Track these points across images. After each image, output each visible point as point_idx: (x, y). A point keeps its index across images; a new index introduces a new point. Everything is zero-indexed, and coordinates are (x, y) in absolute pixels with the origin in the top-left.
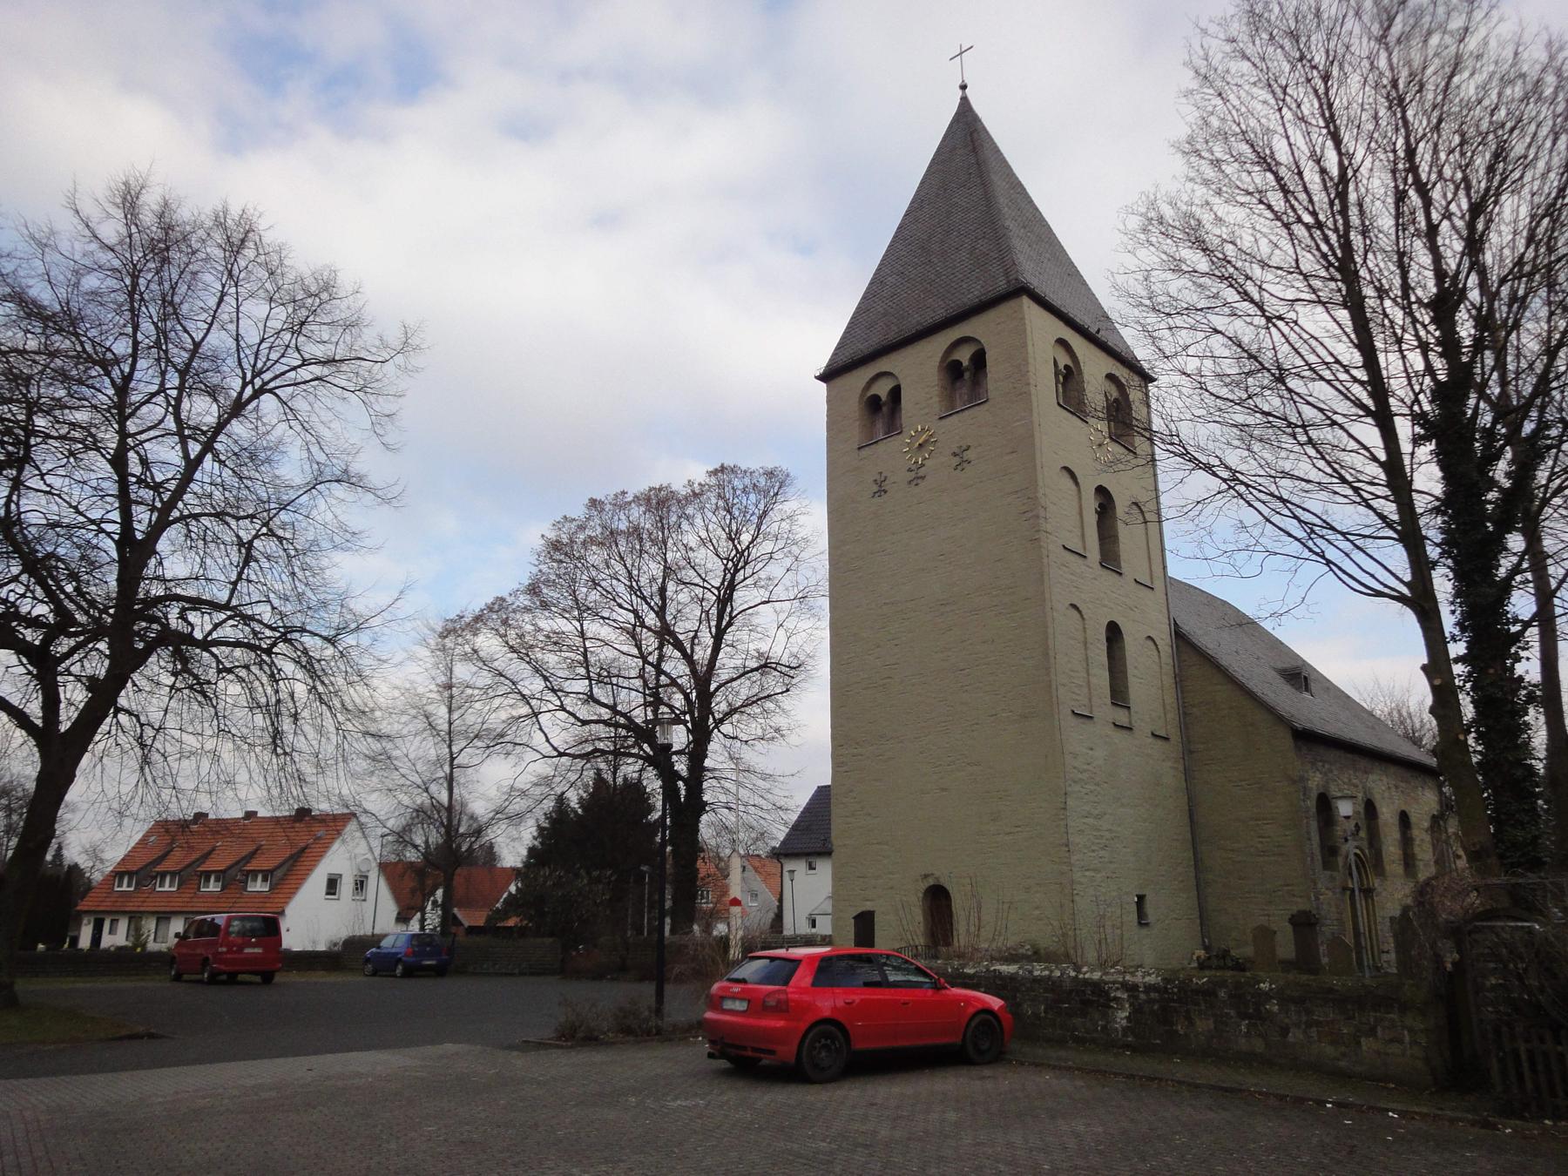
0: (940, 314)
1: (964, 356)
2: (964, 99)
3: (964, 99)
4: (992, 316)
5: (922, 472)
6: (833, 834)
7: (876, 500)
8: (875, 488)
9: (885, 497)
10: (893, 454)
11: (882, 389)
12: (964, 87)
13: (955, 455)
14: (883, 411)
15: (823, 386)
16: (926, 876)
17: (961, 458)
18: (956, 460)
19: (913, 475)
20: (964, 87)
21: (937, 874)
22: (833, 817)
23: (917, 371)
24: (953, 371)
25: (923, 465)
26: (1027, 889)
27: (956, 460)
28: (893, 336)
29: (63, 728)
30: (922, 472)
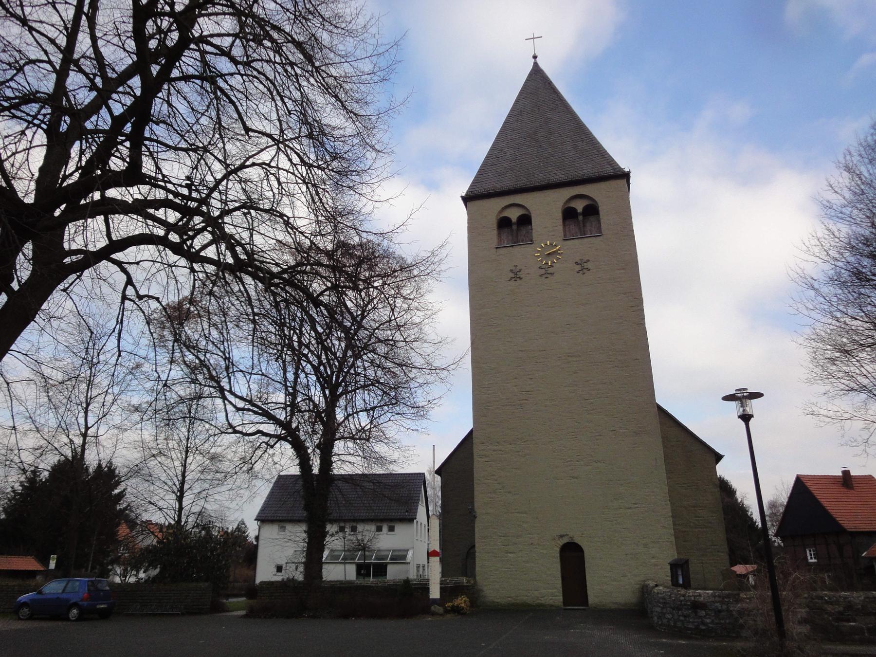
0: (562, 177)
1: (579, 206)
2: (536, 64)
3: (536, 64)
4: (603, 185)
5: (551, 270)
6: (476, 505)
7: (512, 282)
8: (512, 275)
9: (519, 281)
10: (524, 256)
11: (514, 215)
12: (535, 57)
13: (577, 263)
14: (514, 228)
15: (840, 474)
16: (562, 536)
17: (582, 266)
18: (578, 267)
19: (543, 271)
20: (535, 57)
21: (571, 534)
22: (476, 493)
23: (546, 208)
24: (569, 214)
25: (552, 266)
26: (646, 546)
27: (578, 267)
28: (523, 182)
29: (30, 200)
30: (551, 270)
